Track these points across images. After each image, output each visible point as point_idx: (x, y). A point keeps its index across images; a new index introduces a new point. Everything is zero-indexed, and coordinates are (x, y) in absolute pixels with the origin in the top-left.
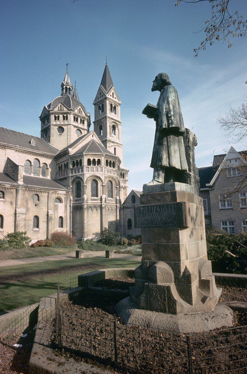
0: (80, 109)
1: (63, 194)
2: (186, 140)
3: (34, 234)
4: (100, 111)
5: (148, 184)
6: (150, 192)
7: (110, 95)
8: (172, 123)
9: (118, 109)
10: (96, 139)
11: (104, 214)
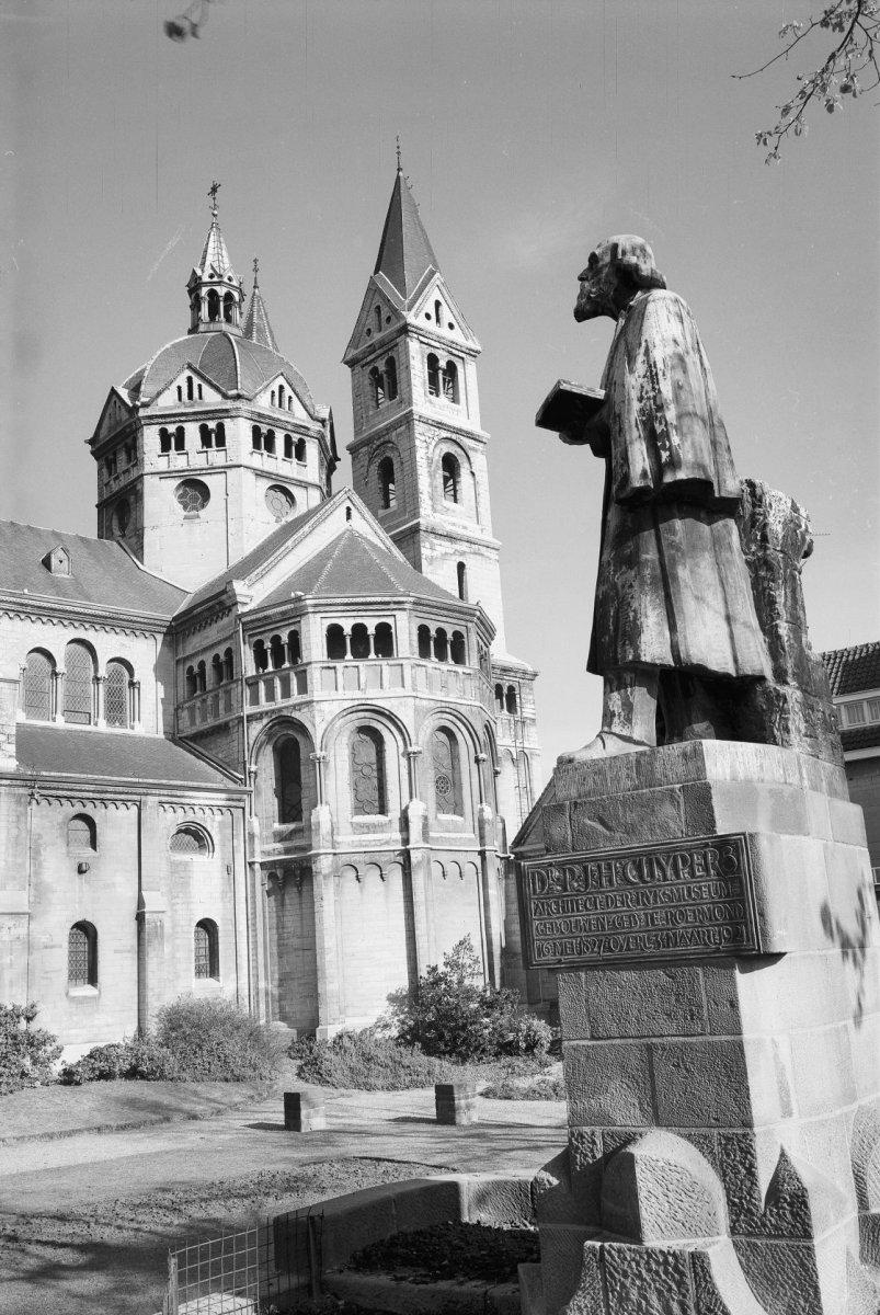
0: (281, 388)
1: (211, 807)
2: (754, 529)
3: (75, 1018)
4: (380, 390)
5: (577, 757)
6: (588, 794)
7: (422, 315)
8: (674, 463)
9: (468, 374)
10: (365, 526)
11: (419, 897)
